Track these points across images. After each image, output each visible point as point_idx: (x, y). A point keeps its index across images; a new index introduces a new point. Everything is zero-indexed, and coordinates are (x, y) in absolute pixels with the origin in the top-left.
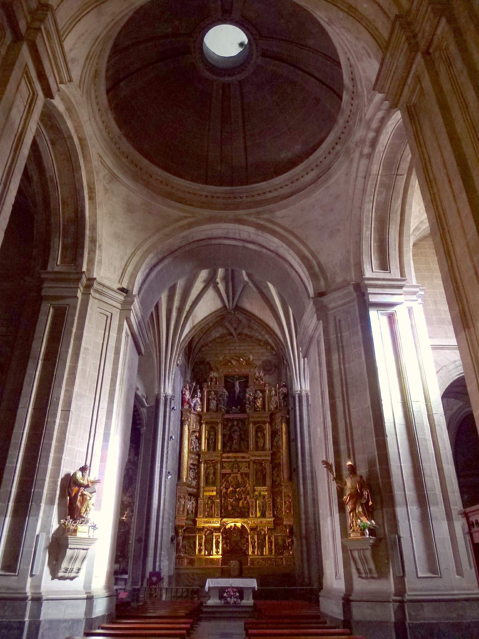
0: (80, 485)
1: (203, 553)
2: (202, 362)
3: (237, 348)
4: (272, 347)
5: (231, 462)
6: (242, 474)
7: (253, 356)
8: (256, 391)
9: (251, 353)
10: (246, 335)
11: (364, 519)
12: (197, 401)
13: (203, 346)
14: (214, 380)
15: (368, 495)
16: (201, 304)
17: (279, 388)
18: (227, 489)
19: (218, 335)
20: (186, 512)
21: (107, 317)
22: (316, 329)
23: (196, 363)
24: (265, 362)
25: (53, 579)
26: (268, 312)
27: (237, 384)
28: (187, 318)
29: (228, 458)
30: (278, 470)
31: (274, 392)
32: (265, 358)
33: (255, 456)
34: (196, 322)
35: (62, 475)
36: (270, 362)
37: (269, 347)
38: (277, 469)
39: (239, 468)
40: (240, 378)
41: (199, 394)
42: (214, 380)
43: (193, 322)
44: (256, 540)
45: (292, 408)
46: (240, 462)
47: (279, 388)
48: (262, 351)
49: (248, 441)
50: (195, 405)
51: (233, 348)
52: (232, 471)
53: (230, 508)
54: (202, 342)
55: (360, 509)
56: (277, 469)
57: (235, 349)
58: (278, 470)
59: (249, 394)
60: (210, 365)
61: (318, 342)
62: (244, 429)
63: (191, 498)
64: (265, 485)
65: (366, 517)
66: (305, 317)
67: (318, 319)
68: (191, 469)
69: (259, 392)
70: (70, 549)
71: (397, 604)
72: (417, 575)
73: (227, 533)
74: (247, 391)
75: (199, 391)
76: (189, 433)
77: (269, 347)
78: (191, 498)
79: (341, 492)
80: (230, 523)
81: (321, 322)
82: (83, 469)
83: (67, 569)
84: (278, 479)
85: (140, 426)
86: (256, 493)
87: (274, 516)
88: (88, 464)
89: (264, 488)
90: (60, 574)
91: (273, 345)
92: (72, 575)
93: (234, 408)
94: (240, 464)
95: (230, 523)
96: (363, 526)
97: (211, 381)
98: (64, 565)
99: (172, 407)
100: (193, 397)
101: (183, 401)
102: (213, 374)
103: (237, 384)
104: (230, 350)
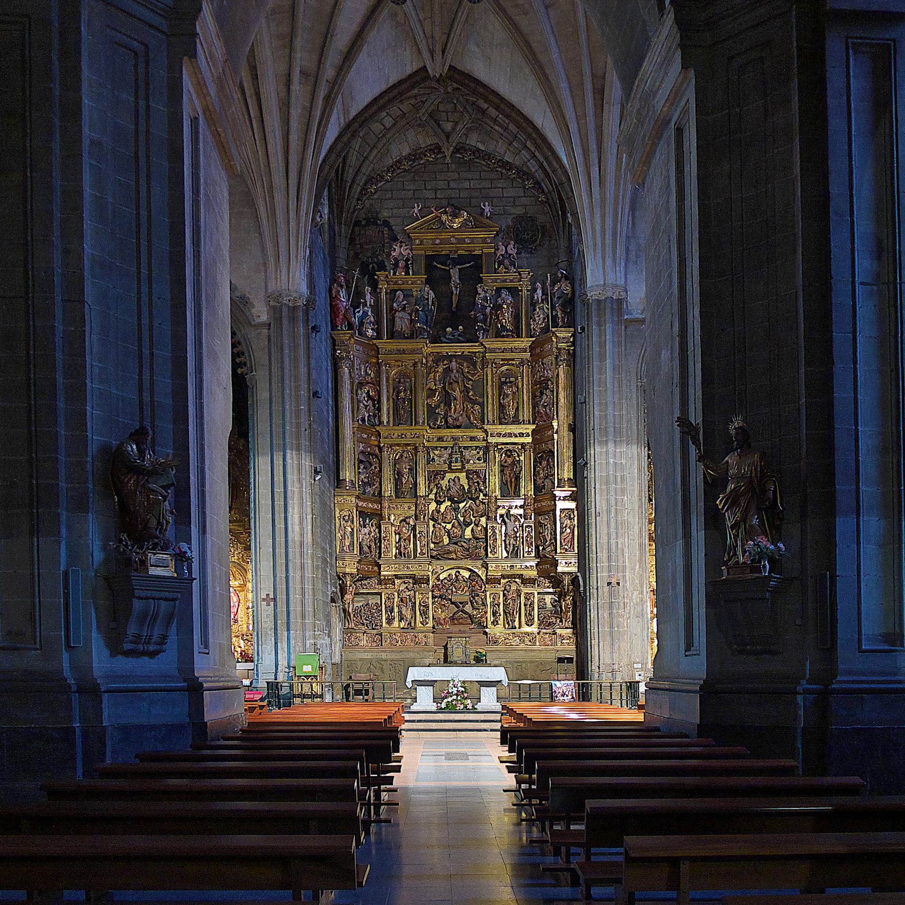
0: (138, 471)
1: (396, 623)
2: (372, 221)
3: (452, 185)
4: (537, 183)
5: (446, 448)
6: (468, 473)
7: (492, 205)
8: (499, 290)
9: (487, 198)
10: (476, 152)
11: (763, 541)
12: (365, 314)
13: (370, 180)
14: (402, 264)
15: (775, 492)
16: (363, 59)
17: (553, 284)
18: (439, 503)
19: (406, 151)
20: (356, 551)
21: (136, 54)
22: (676, 95)
23: (357, 223)
24: (518, 219)
25: (112, 655)
26: (531, 82)
27: (455, 273)
28: (329, 100)
29: (440, 439)
30: (548, 464)
31: (539, 292)
32: (519, 211)
33: (499, 435)
34: (353, 113)
35: (93, 449)
36: (532, 219)
37: (529, 184)
38: (544, 463)
39: (464, 461)
40: (460, 260)
41: (368, 297)
42: (402, 264)
43: (346, 111)
44: (501, 601)
45: (583, 329)
46: (465, 448)
47: (553, 284)
48: (511, 193)
49: (482, 405)
50: (361, 323)
51: (442, 185)
52: (450, 467)
53: (446, 540)
54: (366, 169)
55: (755, 521)
56: (544, 463)
57: (449, 188)
58: (548, 464)
59: (483, 293)
60: (390, 228)
61: (679, 131)
62: (475, 378)
63: (364, 521)
64: (517, 495)
65: (767, 536)
66: (648, 66)
67: (685, 67)
68: (361, 462)
69: (504, 293)
70: (140, 598)
71: (811, 697)
72: (860, 645)
73: (442, 594)
74: (480, 290)
75: (368, 289)
76: (352, 384)
77: (529, 184)
78: (364, 521)
79: (713, 487)
80: (444, 571)
81: (692, 74)
82: (138, 435)
83: (138, 637)
84: (547, 482)
85: (244, 370)
86: (501, 511)
87: (538, 555)
88: (147, 424)
89: (520, 502)
90: (127, 646)
91: (540, 175)
92: (152, 648)
93: (449, 329)
94: (466, 453)
95: (444, 571)
96: (758, 553)
97: (396, 265)
98: (132, 630)
99: (311, 325)
100: (355, 305)
101: (334, 310)
102: (399, 251)
103: (455, 273)
104: (436, 190)
